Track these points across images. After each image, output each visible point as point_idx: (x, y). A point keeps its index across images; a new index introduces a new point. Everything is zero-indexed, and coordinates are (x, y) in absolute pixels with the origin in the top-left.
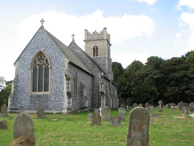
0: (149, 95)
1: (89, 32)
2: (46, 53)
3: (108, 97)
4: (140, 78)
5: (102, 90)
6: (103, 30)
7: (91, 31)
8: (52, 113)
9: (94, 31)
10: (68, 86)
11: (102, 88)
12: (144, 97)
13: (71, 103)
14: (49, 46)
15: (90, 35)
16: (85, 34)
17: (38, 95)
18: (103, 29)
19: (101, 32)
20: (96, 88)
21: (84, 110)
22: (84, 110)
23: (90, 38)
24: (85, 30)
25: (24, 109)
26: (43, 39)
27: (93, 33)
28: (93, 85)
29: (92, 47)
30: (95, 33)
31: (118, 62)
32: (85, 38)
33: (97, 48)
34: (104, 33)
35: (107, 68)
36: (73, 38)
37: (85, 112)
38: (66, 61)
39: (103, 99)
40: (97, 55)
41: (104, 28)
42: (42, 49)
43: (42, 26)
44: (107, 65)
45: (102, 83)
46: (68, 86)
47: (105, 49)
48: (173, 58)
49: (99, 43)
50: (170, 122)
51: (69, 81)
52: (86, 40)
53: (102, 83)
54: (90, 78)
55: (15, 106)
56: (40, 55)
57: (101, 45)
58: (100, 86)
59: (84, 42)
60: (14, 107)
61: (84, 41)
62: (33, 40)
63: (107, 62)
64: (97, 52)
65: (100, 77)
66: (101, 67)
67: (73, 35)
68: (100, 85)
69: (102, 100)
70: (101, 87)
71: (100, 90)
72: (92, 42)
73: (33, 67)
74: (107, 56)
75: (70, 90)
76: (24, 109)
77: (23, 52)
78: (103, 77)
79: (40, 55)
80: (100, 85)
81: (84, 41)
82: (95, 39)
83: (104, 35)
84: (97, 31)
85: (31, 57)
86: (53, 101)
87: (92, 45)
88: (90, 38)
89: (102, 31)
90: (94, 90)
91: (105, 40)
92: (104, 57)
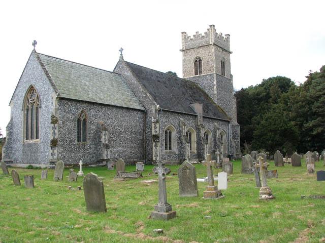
0: (278, 136)
1: (189, 35)
2: (37, 87)
3: (182, 142)
4: (304, 104)
5: (157, 132)
6: (208, 29)
7: (191, 34)
8: (40, 168)
9: (195, 34)
10: (54, 131)
11: (157, 129)
12: (268, 140)
13: (56, 155)
14: (39, 78)
15: (189, 39)
16: (183, 40)
17: (29, 144)
18: (209, 27)
19: (206, 33)
20: (148, 129)
21: (101, 164)
22: (101, 164)
23: (190, 46)
24: (182, 33)
25: (18, 161)
26: (34, 68)
27: (194, 36)
28: (145, 125)
29: (193, 60)
30: (197, 36)
31: (275, 76)
32: (183, 46)
33: (200, 60)
34: (210, 35)
35: (216, 92)
36: (122, 55)
37: (102, 166)
38: (55, 96)
39: (156, 146)
40: (201, 72)
41: (211, 26)
42: (33, 83)
43: (34, 49)
44: (215, 87)
45: (157, 122)
46: (54, 131)
47: (212, 61)
48: (277, 76)
49: (203, 52)
50: (298, 177)
51: (56, 125)
52: (184, 49)
53: (157, 122)
54: (140, 114)
55: (9, 158)
56: (31, 89)
57: (209, 56)
58: (153, 125)
59: (181, 53)
60: (8, 160)
61: (180, 50)
62: (25, 71)
63: (215, 83)
64: (201, 66)
65: (154, 112)
66: (206, 91)
67: (121, 50)
68: (153, 124)
69: (154, 148)
70: (155, 127)
71: (153, 133)
72: (192, 51)
73: (26, 107)
74: (214, 72)
75: (56, 137)
76: (18, 161)
77: (17, 87)
78: (160, 111)
79: (31, 89)
80: (153, 124)
81: (180, 50)
82: (197, 45)
83: (210, 38)
84: (200, 33)
85: (23, 93)
86: (42, 152)
87: (193, 56)
88: (190, 46)
89: (206, 31)
90: (146, 132)
91: (212, 46)
92: (211, 75)
